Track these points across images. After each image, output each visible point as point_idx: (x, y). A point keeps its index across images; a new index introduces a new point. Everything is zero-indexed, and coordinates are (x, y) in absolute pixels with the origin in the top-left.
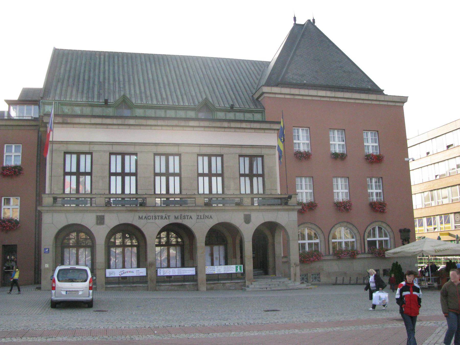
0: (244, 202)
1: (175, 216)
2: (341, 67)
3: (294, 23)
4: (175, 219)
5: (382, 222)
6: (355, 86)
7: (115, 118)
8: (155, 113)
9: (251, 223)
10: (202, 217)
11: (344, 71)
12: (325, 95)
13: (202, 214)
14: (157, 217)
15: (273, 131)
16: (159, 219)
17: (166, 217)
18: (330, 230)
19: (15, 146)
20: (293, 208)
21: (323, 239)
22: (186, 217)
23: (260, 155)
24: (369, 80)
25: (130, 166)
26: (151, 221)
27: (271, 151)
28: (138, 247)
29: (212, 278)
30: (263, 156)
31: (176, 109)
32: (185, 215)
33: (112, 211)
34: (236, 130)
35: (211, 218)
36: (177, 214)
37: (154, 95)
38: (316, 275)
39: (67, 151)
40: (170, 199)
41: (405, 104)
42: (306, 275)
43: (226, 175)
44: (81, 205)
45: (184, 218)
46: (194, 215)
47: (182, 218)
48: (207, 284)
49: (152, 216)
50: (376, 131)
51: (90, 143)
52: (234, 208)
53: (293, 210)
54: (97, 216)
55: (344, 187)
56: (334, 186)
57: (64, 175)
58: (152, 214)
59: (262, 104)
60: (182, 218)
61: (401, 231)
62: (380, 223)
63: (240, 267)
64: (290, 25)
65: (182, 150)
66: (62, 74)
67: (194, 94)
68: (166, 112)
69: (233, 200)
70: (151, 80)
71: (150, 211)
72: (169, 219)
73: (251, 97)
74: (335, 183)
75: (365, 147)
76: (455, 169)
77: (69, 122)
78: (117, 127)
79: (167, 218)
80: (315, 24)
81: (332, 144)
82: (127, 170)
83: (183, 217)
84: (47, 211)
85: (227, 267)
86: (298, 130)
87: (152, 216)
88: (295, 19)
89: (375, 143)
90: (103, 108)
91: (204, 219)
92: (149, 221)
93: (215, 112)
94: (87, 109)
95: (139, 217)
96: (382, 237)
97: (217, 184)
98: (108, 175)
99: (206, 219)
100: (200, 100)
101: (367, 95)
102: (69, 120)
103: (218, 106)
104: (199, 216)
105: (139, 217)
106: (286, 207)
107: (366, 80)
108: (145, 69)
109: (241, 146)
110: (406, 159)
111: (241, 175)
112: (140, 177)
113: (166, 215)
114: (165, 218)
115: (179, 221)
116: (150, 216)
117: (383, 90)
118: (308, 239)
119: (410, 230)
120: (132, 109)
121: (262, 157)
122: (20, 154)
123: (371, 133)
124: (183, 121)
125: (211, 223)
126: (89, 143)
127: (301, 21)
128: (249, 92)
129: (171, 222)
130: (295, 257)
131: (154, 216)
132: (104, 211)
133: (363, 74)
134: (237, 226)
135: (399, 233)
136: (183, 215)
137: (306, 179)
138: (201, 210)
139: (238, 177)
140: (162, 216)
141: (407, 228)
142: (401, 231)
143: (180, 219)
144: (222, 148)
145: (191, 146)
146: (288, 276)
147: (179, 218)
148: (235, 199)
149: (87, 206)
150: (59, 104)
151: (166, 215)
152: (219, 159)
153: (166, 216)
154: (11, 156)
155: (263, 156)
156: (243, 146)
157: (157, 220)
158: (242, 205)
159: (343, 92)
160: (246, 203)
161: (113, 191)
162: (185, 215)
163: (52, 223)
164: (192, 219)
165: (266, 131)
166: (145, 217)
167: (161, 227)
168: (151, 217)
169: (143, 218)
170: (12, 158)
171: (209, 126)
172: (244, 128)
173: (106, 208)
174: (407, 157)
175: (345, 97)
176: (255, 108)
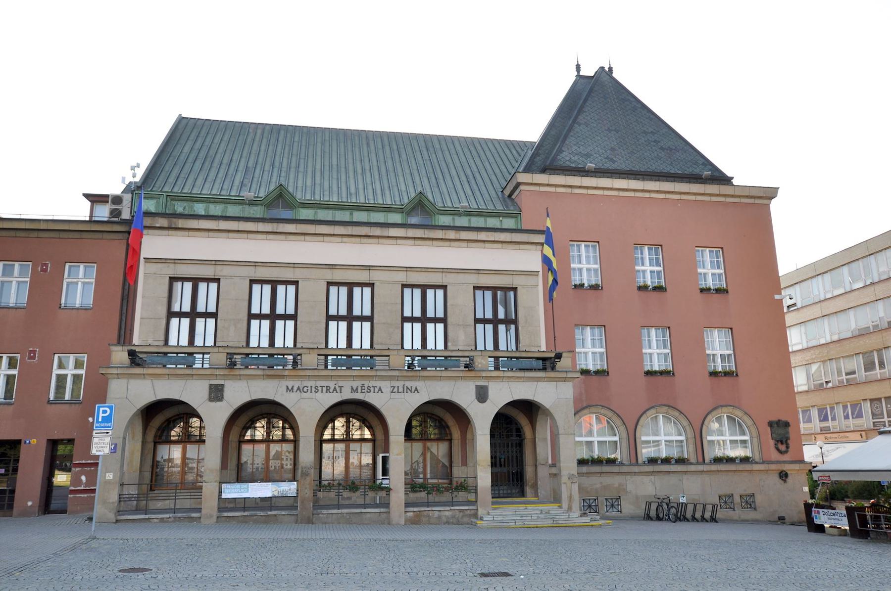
0: (477, 364)
1: (352, 387)
3: (576, 73)
5: (602, 406)
6: (680, 172)
10: (401, 389)
11: (662, 147)
12: (626, 187)
13: (400, 384)
14: (320, 389)
15: (534, 247)
16: (322, 392)
17: (335, 389)
19: (85, 267)
20: (564, 375)
21: (625, 435)
22: (372, 389)
23: (511, 286)
24: (706, 162)
26: (309, 394)
27: (530, 280)
28: (373, 441)
30: (446, 286)
31: (470, 215)
32: (371, 385)
33: (239, 377)
34: (470, 244)
35: (416, 392)
36: (356, 384)
37: (335, 188)
38: (614, 501)
39: (175, 276)
42: (617, 499)
43: (450, 320)
44: (275, 367)
45: (368, 392)
46: (386, 385)
47: (363, 391)
49: (311, 387)
50: (658, 245)
51: (216, 262)
52: (462, 374)
53: (565, 379)
55: (597, 343)
56: (643, 342)
57: (402, 321)
59: (517, 204)
60: (363, 391)
61: (771, 424)
62: (730, 409)
64: (570, 78)
65: (375, 276)
67: (403, 188)
68: (351, 214)
69: (457, 360)
71: (308, 377)
72: (341, 392)
73: (500, 194)
74: (645, 338)
75: (699, 276)
77: (180, 226)
78: (339, 239)
79: (338, 389)
80: (614, 75)
81: (574, 269)
82: (430, 314)
83: (366, 389)
86: (579, 246)
87: (311, 387)
88: (578, 67)
89: (718, 268)
91: (404, 392)
92: (304, 395)
93: (437, 216)
95: (288, 388)
97: (435, 333)
98: (246, 318)
100: (413, 195)
101: (704, 185)
102: (181, 223)
103: (442, 205)
104: (394, 387)
105: (288, 388)
107: (701, 161)
110: (777, 297)
111: (477, 321)
112: (301, 322)
113: (335, 384)
114: (334, 390)
115: (359, 396)
116: (308, 387)
117: (732, 178)
119: (788, 423)
120: (295, 210)
121: (515, 289)
122: (28, 279)
123: (710, 251)
124: (379, 228)
125: (417, 400)
126: (214, 263)
127: (589, 71)
128: (497, 185)
130: (569, 466)
131: (314, 386)
132: (224, 376)
133: (694, 153)
134: (378, 407)
136: (366, 386)
137: (594, 330)
138: (398, 376)
139: (473, 323)
140: (329, 387)
141: (784, 419)
142: (771, 424)
143: (362, 392)
144: (444, 274)
145: (458, 272)
146: (556, 499)
148: (462, 359)
149: (287, 368)
151: (335, 384)
152: (367, 291)
153: (335, 388)
154: (77, 284)
155: (446, 286)
156: (481, 272)
157: (319, 394)
158: (472, 369)
159: (659, 181)
160: (480, 365)
161: (332, 344)
165: (522, 246)
166: (298, 388)
168: (309, 388)
169: (295, 389)
170: (12, 286)
171: (424, 237)
172: (484, 241)
173: (226, 372)
175: (708, 192)
176: (504, 210)
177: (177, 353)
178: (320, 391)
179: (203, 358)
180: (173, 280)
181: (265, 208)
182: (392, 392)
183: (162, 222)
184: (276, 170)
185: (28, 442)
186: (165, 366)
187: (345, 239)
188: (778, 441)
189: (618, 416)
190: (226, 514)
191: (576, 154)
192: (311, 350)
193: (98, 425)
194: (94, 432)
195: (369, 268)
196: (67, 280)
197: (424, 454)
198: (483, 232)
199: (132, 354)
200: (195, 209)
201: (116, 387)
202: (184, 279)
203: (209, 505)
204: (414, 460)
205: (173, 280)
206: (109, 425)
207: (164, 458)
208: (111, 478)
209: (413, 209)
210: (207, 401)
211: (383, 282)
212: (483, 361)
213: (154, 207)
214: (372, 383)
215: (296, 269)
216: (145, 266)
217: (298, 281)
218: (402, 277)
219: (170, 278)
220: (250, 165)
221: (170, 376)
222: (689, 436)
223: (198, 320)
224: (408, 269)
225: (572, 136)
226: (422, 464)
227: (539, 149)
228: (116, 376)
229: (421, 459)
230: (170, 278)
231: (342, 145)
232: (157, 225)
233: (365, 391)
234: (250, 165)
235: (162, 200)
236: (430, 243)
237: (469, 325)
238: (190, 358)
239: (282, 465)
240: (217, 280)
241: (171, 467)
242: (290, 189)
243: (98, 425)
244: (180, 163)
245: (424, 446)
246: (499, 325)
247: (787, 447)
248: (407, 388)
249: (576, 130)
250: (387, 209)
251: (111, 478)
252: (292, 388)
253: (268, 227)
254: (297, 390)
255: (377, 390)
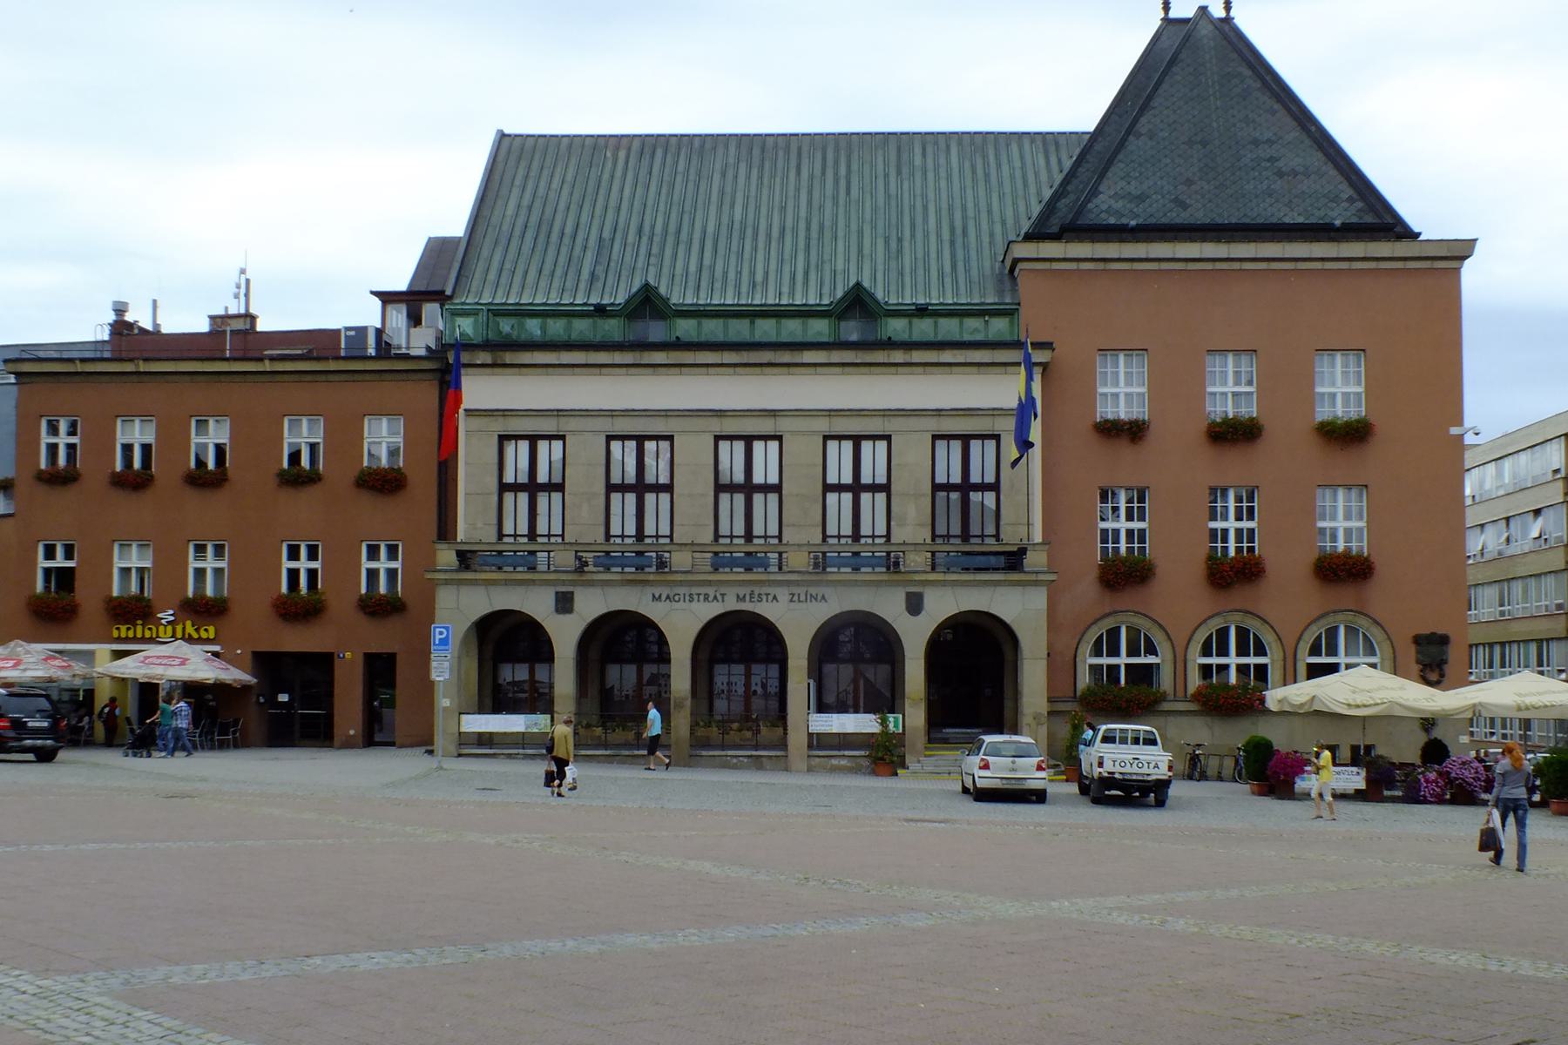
2: (1272, 159)
4: (653, 600)
7: (618, 350)
8: (726, 327)
9: (923, 613)
12: (1197, 256)
13: (801, 590)
14: (696, 597)
17: (715, 598)
18: (1298, 635)
20: (1033, 577)
21: (1169, 656)
25: (657, 470)
26: (681, 605)
29: (819, 742)
33: (591, 584)
36: (742, 591)
40: (612, 554)
41: (1466, 261)
45: (758, 601)
46: (783, 594)
48: (809, 756)
49: (684, 595)
51: (559, 413)
53: (1036, 583)
54: (557, 593)
58: (682, 590)
61: (1418, 640)
63: (896, 720)
66: (508, 219)
68: (752, 323)
70: (737, 226)
72: (723, 601)
73: (1008, 263)
76: (898, 525)
77: (508, 362)
78: (974, 369)
79: (719, 597)
84: (447, 582)
85: (1426, 808)
87: (684, 595)
90: (596, 318)
94: (558, 324)
96: (1358, 655)
98: (603, 491)
99: (811, 601)
102: (509, 357)
105: (654, 596)
106: (1015, 576)
108: (728, 189)
109: (938, 413)
110: (1454, 431)
118: (1129, 655)
124: (788, 352)
129: (729, 609)
132: (574, 583)
135: (1412, 649)
136: (756, 593)
141: (1440, 632)
142: (1418, 640)
143: (751, 601)
144: (886, 418)
147: (748, 598)
150: (490, 314)
154: (380, 443)
157: (695, 605)
162: (762, 592)
163: (458, 608)
164: (777, 601)
166: (668, 597)
167: (705, 622)
169: (664, 597)
174: (1460, 422)
177: (515, 552)
178: (764, 599)
179: (549, 557)
180: (503, 439)
181: (626, 322)
182: (791, 601)
183: (484, 357)
184: (645, 239)
185: (341, 655)
186: (500, 568)
187: (738, 370)
188: (1424, 665)
189: (1160, 625)
190: (583, 752)
191: (1122, 198)
192: (683, 547)
193: (435, 648)
194: (432, 655)
195: (773, 413)
196: (368, 440)
197: (855, 681)
198: (947, 351)
199: (461, 555)
200: (527, 327)
201: (446, 599)
202: (517, 437)
203: (797, 739)
204: (841, 690)
205: (503, 439)
206: (446, 648)
207: (508, 681)
208: (448, 705)
209: (848, 308)
210: (555, 613)
211: (792, 433)
212: (917, 558)
213: (471, 327)
214: (765, 590)
215: (670, 420)
216: (466, 420)
217: (673, 436)
218: (823, 425)
219: (500, 436)
220: (606, 235)
221: (507, 583)
222: (1275, 657)
223: (540, 494)
224: (832, 413)
225: (1120, 161)
226: (852, 695)
227: (1068, 183)
228: (444, 582)
229: (851, 688)
230: (500, 436)
231: (755, 172)
232: (479, 362)
233: (755, 599)
234: (606, 235)
235: (482, 317)
236: (866, 369)
237: (923, 495)
238: (531, 558)
239: (660, 692)
240: (562, 438)
241: (517, 692)
242: (663, 290)
243: (435, 648)
244: (503, 241)
245: (856, 671)
246: (971, 493)
247: (1442, 675)
248: (811, 595)
249: (1129, 148)
250: (805, 313)
251: (448, 705)
252: (660, 596)
253: (628, 358)
254: (667, 599)
255: (770, 598)
